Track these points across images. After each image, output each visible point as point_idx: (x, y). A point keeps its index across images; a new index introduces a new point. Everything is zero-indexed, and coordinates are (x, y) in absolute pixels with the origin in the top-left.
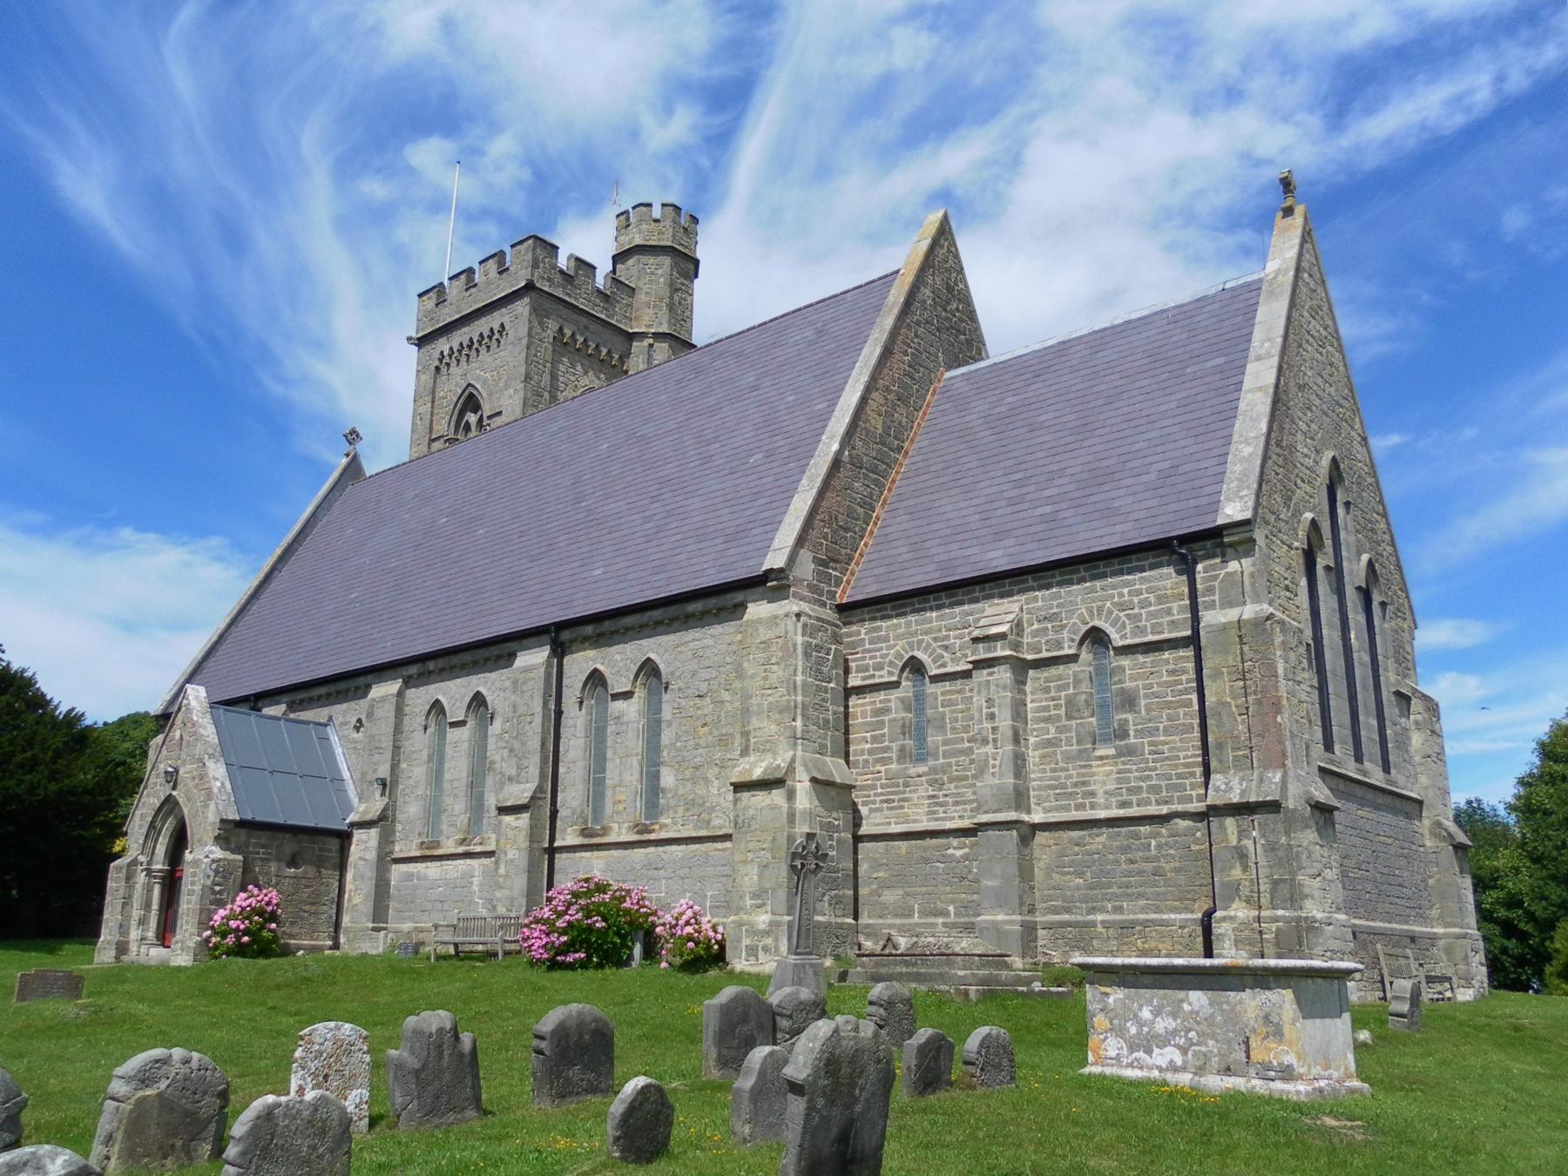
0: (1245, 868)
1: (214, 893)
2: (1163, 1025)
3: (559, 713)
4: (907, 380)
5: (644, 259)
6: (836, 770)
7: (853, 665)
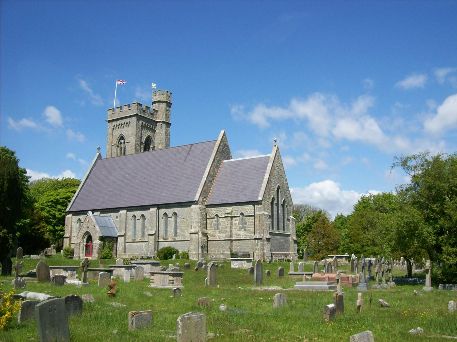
0: (258, 246)
1: (99, 248)
2: (237, 264)
3: (159, 219)
4: (217, 164)
5: (160, 104)
6: (205, 231)
7: (207, 214)
